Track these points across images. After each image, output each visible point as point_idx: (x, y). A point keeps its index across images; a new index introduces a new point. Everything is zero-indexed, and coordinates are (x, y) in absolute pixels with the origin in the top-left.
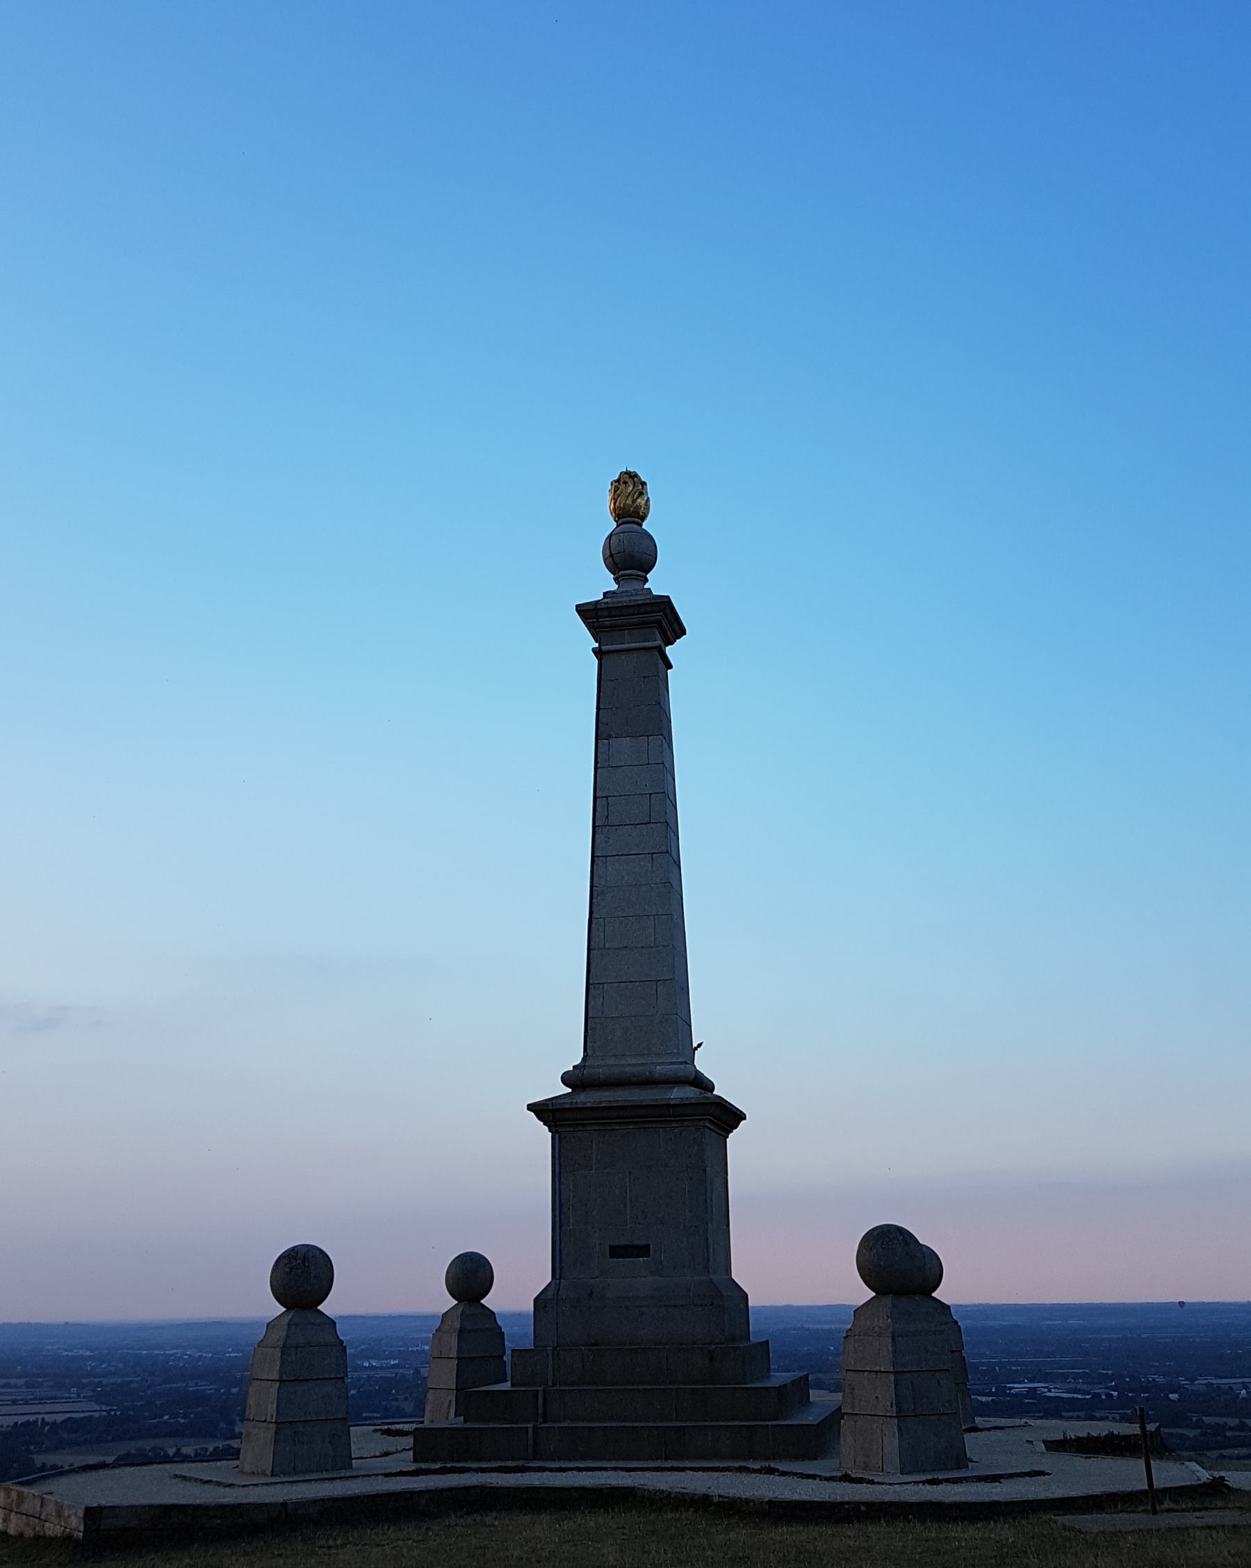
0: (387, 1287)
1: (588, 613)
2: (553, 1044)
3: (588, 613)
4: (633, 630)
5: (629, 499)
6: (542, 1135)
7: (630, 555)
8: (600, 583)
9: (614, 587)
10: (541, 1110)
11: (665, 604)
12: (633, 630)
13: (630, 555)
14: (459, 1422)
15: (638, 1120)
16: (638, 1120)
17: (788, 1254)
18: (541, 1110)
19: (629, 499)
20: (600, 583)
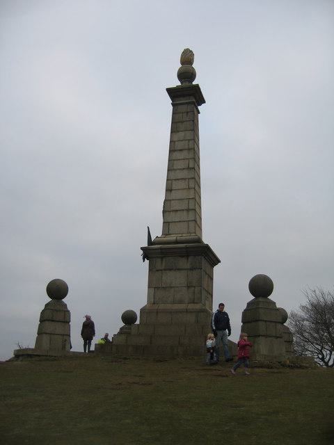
0: (30, 347)
1: (170, 91)
2: (149, 216)
3: (170, 91)
4: (186, 97)
5: (187, 58)
6: (142, 252)
7: (187, 74)
8: (176, 83)
9: (179, 84)
10: (142, 249)
11: (197, 86)
12: (186, 97)
13: (187, 74)
14: (179, 84)
15: (180, 255)
16: (180, 255)
17: (229, 292)
18: (142, 249)
19: (187, 58)
20: (176, 83)
